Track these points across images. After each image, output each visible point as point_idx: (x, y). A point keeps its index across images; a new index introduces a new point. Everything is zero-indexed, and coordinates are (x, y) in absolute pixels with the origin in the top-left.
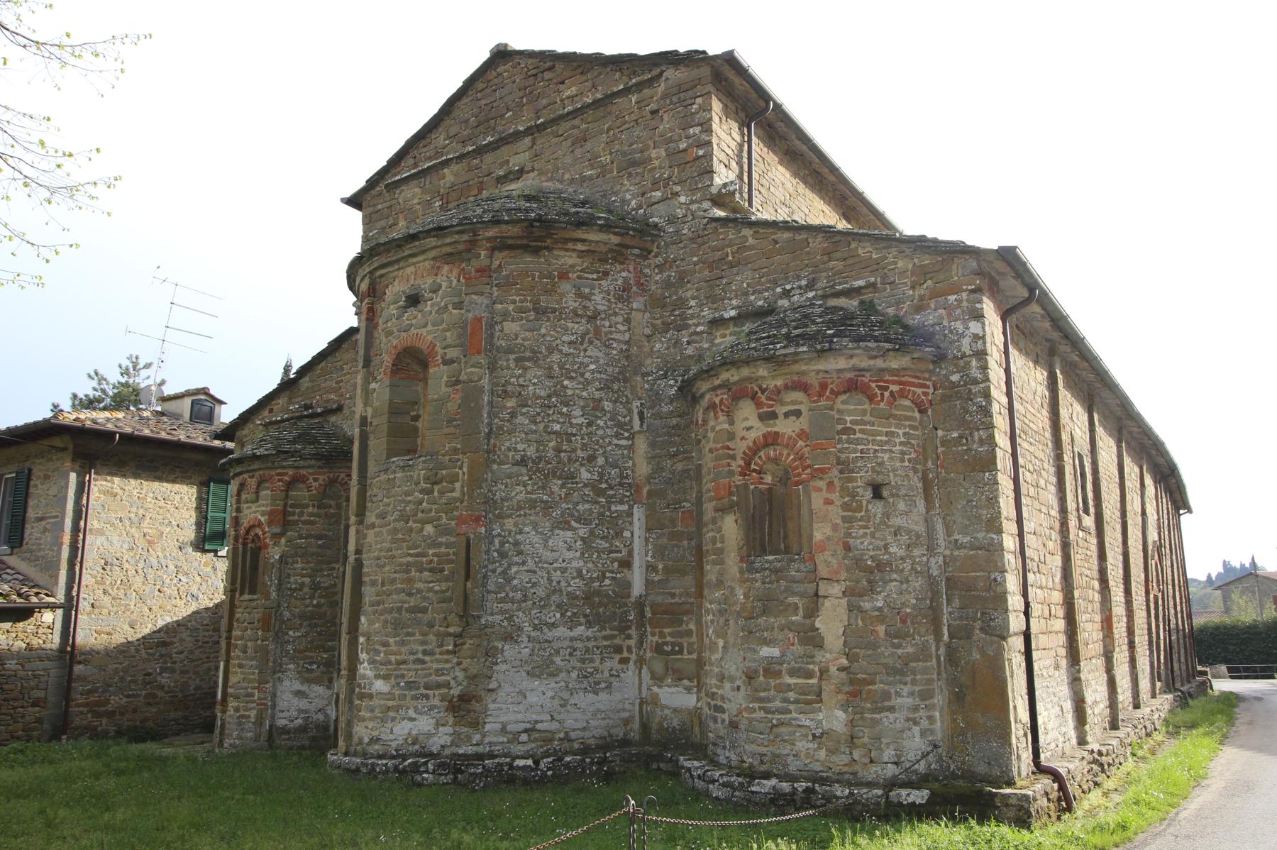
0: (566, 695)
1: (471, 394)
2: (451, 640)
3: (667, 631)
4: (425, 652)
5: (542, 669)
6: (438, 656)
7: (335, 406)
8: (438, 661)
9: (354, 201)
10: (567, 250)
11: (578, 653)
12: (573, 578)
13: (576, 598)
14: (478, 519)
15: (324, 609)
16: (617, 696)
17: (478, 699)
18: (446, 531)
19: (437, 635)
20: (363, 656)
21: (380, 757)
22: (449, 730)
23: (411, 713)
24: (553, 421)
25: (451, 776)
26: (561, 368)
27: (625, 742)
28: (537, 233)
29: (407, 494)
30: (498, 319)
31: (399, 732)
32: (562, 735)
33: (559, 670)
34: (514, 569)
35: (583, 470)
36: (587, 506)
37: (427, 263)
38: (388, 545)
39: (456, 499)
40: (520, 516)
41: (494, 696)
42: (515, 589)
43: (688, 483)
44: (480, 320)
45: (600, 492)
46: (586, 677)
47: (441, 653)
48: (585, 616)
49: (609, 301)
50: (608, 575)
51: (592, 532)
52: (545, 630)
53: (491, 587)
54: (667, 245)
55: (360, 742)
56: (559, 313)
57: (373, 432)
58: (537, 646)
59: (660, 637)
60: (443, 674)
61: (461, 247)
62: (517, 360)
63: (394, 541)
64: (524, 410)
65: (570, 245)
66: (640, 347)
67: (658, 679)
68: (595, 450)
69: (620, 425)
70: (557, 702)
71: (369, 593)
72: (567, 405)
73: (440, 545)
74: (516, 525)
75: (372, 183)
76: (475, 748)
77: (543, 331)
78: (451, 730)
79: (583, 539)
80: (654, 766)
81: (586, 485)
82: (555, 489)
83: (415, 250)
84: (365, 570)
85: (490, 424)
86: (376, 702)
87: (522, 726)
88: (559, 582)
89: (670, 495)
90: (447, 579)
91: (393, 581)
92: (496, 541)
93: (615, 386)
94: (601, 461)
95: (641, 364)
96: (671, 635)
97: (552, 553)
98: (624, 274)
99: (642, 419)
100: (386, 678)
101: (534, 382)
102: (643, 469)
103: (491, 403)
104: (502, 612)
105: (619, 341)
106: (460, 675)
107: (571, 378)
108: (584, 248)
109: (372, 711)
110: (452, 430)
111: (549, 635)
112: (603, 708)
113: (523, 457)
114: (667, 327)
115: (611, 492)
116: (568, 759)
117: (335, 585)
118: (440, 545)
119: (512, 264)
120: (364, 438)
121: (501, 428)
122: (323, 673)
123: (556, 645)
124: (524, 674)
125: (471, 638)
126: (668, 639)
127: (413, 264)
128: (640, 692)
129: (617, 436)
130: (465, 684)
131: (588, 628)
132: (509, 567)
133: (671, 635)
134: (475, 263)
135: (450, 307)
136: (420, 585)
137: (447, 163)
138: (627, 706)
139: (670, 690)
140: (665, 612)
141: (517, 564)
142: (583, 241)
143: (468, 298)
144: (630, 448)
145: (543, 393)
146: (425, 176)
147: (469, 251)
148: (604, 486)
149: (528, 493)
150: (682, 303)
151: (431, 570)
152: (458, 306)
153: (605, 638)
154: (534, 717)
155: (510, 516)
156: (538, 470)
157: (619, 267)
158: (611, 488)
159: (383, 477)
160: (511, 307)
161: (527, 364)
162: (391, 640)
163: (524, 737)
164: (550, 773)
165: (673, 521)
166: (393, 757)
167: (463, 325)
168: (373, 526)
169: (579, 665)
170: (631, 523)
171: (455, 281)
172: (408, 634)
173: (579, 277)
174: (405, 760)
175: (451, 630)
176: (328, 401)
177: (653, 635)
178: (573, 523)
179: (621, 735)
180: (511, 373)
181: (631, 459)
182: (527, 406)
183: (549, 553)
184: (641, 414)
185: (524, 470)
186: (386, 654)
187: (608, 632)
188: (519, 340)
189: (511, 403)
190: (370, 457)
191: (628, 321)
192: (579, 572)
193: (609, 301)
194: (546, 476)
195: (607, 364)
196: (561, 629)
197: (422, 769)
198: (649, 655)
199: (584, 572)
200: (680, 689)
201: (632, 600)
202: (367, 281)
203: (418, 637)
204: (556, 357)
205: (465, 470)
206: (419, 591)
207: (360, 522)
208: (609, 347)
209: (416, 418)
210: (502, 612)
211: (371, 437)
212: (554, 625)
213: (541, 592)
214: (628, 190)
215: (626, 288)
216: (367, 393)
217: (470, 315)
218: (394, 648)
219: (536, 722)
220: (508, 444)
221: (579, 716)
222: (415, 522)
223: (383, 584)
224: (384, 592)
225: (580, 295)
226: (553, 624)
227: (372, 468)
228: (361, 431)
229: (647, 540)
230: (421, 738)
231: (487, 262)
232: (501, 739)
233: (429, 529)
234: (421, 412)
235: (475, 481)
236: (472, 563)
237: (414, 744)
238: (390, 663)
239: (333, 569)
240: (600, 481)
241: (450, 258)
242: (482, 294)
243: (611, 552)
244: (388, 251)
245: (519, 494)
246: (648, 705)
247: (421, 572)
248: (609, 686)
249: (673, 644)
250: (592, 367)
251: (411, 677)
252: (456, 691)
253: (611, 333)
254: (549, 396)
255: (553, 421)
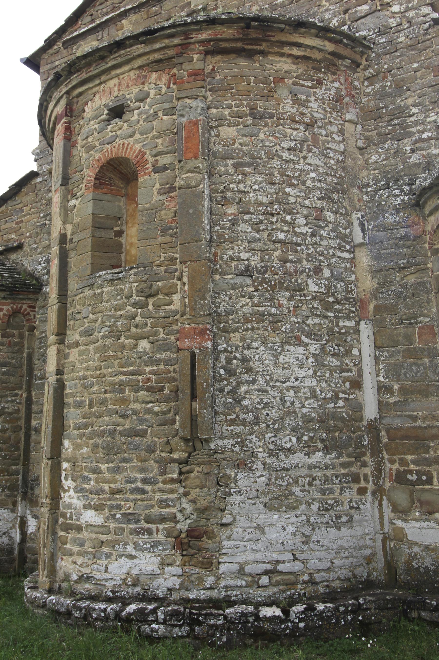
0: (307, 531)
1: (190, 195)
2: (175, 467)
3: (409, 458)
4: (145, 481)
5: (280, 500)
6: (160, 485)
7: (15, 245)
8: (162, 491)
9: (33, 62)
10: (282, 55)
11: (317, 482)
12: (307, 398)
13: (311, 420)
14: (202, 333)
15: (8, 433)
16: (358, 531)
17: (211, 536)
18: (165, 347)
19: (159, 461)
20: (67, 483)
21: (94, 598)
22: (177, 570)
23: (130, 549)
24: (277, 229)
25: (186, 629)
26: (282, 175)
27: (369, 584)
28: (253, 34)
29: (117, 308)
30: (214, 124)
31: (116, 570)
32: (306, 578)
33: (299, 502)
34: (244, 388)
35: (310, 282)
36: (317, 320)
37: (132, 73)
38: (97, 364)
39: (175, 313)
40: (247, 330)
41: (229, 532)
42: (245, 410)
43: (424, 297)
44: (196, 123)
45: (328, 306)
46: (327, 510)
47: (164, 482)
48: (322, 441)
49: (324, 109)
50: (341, 395)
51: (323, 348)
52: (282, 456)
53: (219, 408)
54: (379, 56)
55: (67, 578)
56: (279, 119)
57: (74, 249)
58: (274, 475)
59: (401, 465)
60: (168, 506)
61: (171, 52)
62: (235, 166)
63: (103, 359)
64: (246, 217)
65: (286, 50)
66: (354, 159)
67: (403, 513)
68: (321, 261)
69: (343, 237)
70: (299, 539)
71: (73, 416)
72: (290, 213)
73: (159, 361)
74: (243, 339)
75: (50, 42)
76: (208, 593)
77: (262, 136)
78: (179, 571)
79: (314, 355)
80: (414, 614)
81: (314, 298)
82: (283, 301)
83: (119, 60)
84: (68, 391)
85: (211, 232)
86: (85, 535)
87: (263, 567)
88: (292, 403)
89: (403, 310)
90: (167, 400)
91: (103, 402)
92: (223, 357)
93: (335, 197)
94: (326, 273)
95: (356, 177)
96: (414, 462)
97: (286, 373)
98: (336, 85)
99: (363, 231)
100: (98, 508)
101: (256, 189)
102: (368, 283)
103: (210, 209)
104: (233, 436)
105: (335, 151)
106: (188, 507)
107: (293, 186)
108: (300, 53)
109: (82, 545)
110: (168, 239)
111: (287, 462)
112: (345, 545)
113: (247, 267)
114: (383, 137)
115: (338, 307)
116: (320, 607)
117: (18, 411)
118: (159, 361)
119: (227, 68)
120: (64, 257)
121: (222, 236)
122: (7, 496)
123: (294, 473)
124: (262, 507)
125: (199, 464)
126: (412, 466)
127: (117, 76)
128: (382, 526)
129: (340, 248)
130: (194, 517)
131: (325, 454)
132: (239, 384)
133: (414, 462)
134: (187, 66)
135: (160, 114)
136: (137, 406)
137: (125, 14)
138: (369, 542)
139: (418, 525)
140: (406, 437)
141: (247, 382)
142: (299, 45)
143: (181, 102)
144: (352, 261)
145: (265, 200)
146: (103, 30)
147: (180, 55)
148: (331, 299)
149: (254, 305)
150: (402, 112)
151: (148, 390)
152: (170, 111)
153: (344, 465)
154: (275, 557)
155: (236, 330)
156: (264, 281)
157: (331, 77)
158: (337, 302)
159: (87, 293)
160: (227, 112)
161: (248, 170)
162: (104, 467)
163: (265, 580)
164: (302, 625)
165: (409, 339)
166: (109, 600)
167: (175, 132)
168: (77, 344)
169: (319, 496)
170: (359, 341)
171: (164, 89)
172: (124, 460)
173: (295, 84)
174: (125, 604)
175: (175, 456)
176: (8, 241)
177: (392, 462)
178: (303, 338)
179: (365, 575)
180: (229, 177)
181: (353, 272)
182: (249, 213)
183: (280, 371)
184: (362, 225)
185: (248, 281)
186: (96, 480)
187: (345, 459)
188: (237, 146)
189: (232, 210)
190: (70, 274)
191: (341, 132)
192: (313, 391)
193: (324, 109)
194: (273, 288)
195: (326, 174)
196: (299, 455)
197: (150, 618)
198: (388, 484)
199: (318, 392)
200: (432, 524)
201: (365, 423)
202: (63, 102)
203: (135, 463)
204: (276, 163)
205: (185, 280)
206: (135, 413)
207: (61, 342)
208: (326, 156)
209: (120, 233)
210: (233, 436)
211: (72, 254)
212: (289, 451)
213: (274, 413)
214: (327, 10)
215: (339, 99)
216: (66, 212)
217: (184, 120)
218: (107, 475)
219: (278, 562)
220: (230, 253)
221: (322, 554)
222: (127, 338)
223: (91, 405)
224: (93, 414)
225: (296, 101)
226: (289, 450)
227: (73, 284)
228: (61, 248)
229: (377, 358)
230: (142, 579)
231: (200, 65)
232: (239, 582)
233: (144, 345)
234: (124, 228)
235: (197, 292)
236: (198, 380)
237: (134, 585)
238: (102, 492)
239: (17, 395)
240: (327, 294)
241: (158, 65)
242: (196, 98)
243: (342, 371)
244: (89, 65)
245: (245, 307)
246: (391, 540)
247: (137, 391)
248: (350, 520)
249: (419, 473)
250: (313, 175)
251: (129, 507)
252: (183, 526)
253: (328, 142)
254: (272, 203)
255: (277, 229)
